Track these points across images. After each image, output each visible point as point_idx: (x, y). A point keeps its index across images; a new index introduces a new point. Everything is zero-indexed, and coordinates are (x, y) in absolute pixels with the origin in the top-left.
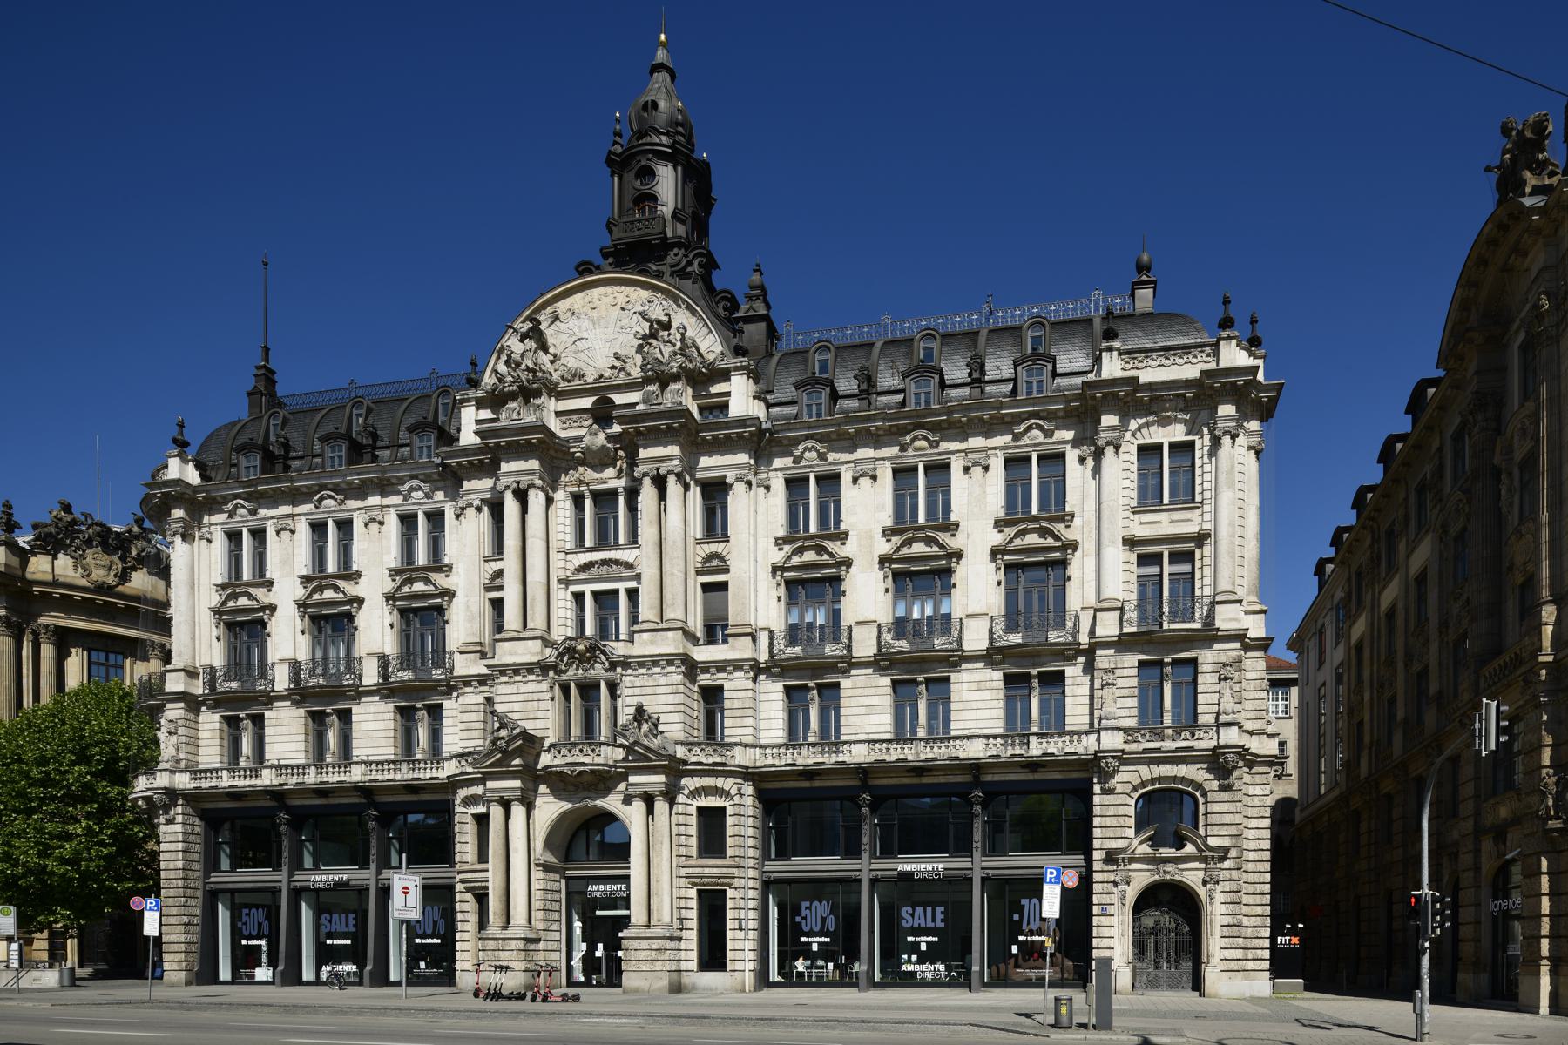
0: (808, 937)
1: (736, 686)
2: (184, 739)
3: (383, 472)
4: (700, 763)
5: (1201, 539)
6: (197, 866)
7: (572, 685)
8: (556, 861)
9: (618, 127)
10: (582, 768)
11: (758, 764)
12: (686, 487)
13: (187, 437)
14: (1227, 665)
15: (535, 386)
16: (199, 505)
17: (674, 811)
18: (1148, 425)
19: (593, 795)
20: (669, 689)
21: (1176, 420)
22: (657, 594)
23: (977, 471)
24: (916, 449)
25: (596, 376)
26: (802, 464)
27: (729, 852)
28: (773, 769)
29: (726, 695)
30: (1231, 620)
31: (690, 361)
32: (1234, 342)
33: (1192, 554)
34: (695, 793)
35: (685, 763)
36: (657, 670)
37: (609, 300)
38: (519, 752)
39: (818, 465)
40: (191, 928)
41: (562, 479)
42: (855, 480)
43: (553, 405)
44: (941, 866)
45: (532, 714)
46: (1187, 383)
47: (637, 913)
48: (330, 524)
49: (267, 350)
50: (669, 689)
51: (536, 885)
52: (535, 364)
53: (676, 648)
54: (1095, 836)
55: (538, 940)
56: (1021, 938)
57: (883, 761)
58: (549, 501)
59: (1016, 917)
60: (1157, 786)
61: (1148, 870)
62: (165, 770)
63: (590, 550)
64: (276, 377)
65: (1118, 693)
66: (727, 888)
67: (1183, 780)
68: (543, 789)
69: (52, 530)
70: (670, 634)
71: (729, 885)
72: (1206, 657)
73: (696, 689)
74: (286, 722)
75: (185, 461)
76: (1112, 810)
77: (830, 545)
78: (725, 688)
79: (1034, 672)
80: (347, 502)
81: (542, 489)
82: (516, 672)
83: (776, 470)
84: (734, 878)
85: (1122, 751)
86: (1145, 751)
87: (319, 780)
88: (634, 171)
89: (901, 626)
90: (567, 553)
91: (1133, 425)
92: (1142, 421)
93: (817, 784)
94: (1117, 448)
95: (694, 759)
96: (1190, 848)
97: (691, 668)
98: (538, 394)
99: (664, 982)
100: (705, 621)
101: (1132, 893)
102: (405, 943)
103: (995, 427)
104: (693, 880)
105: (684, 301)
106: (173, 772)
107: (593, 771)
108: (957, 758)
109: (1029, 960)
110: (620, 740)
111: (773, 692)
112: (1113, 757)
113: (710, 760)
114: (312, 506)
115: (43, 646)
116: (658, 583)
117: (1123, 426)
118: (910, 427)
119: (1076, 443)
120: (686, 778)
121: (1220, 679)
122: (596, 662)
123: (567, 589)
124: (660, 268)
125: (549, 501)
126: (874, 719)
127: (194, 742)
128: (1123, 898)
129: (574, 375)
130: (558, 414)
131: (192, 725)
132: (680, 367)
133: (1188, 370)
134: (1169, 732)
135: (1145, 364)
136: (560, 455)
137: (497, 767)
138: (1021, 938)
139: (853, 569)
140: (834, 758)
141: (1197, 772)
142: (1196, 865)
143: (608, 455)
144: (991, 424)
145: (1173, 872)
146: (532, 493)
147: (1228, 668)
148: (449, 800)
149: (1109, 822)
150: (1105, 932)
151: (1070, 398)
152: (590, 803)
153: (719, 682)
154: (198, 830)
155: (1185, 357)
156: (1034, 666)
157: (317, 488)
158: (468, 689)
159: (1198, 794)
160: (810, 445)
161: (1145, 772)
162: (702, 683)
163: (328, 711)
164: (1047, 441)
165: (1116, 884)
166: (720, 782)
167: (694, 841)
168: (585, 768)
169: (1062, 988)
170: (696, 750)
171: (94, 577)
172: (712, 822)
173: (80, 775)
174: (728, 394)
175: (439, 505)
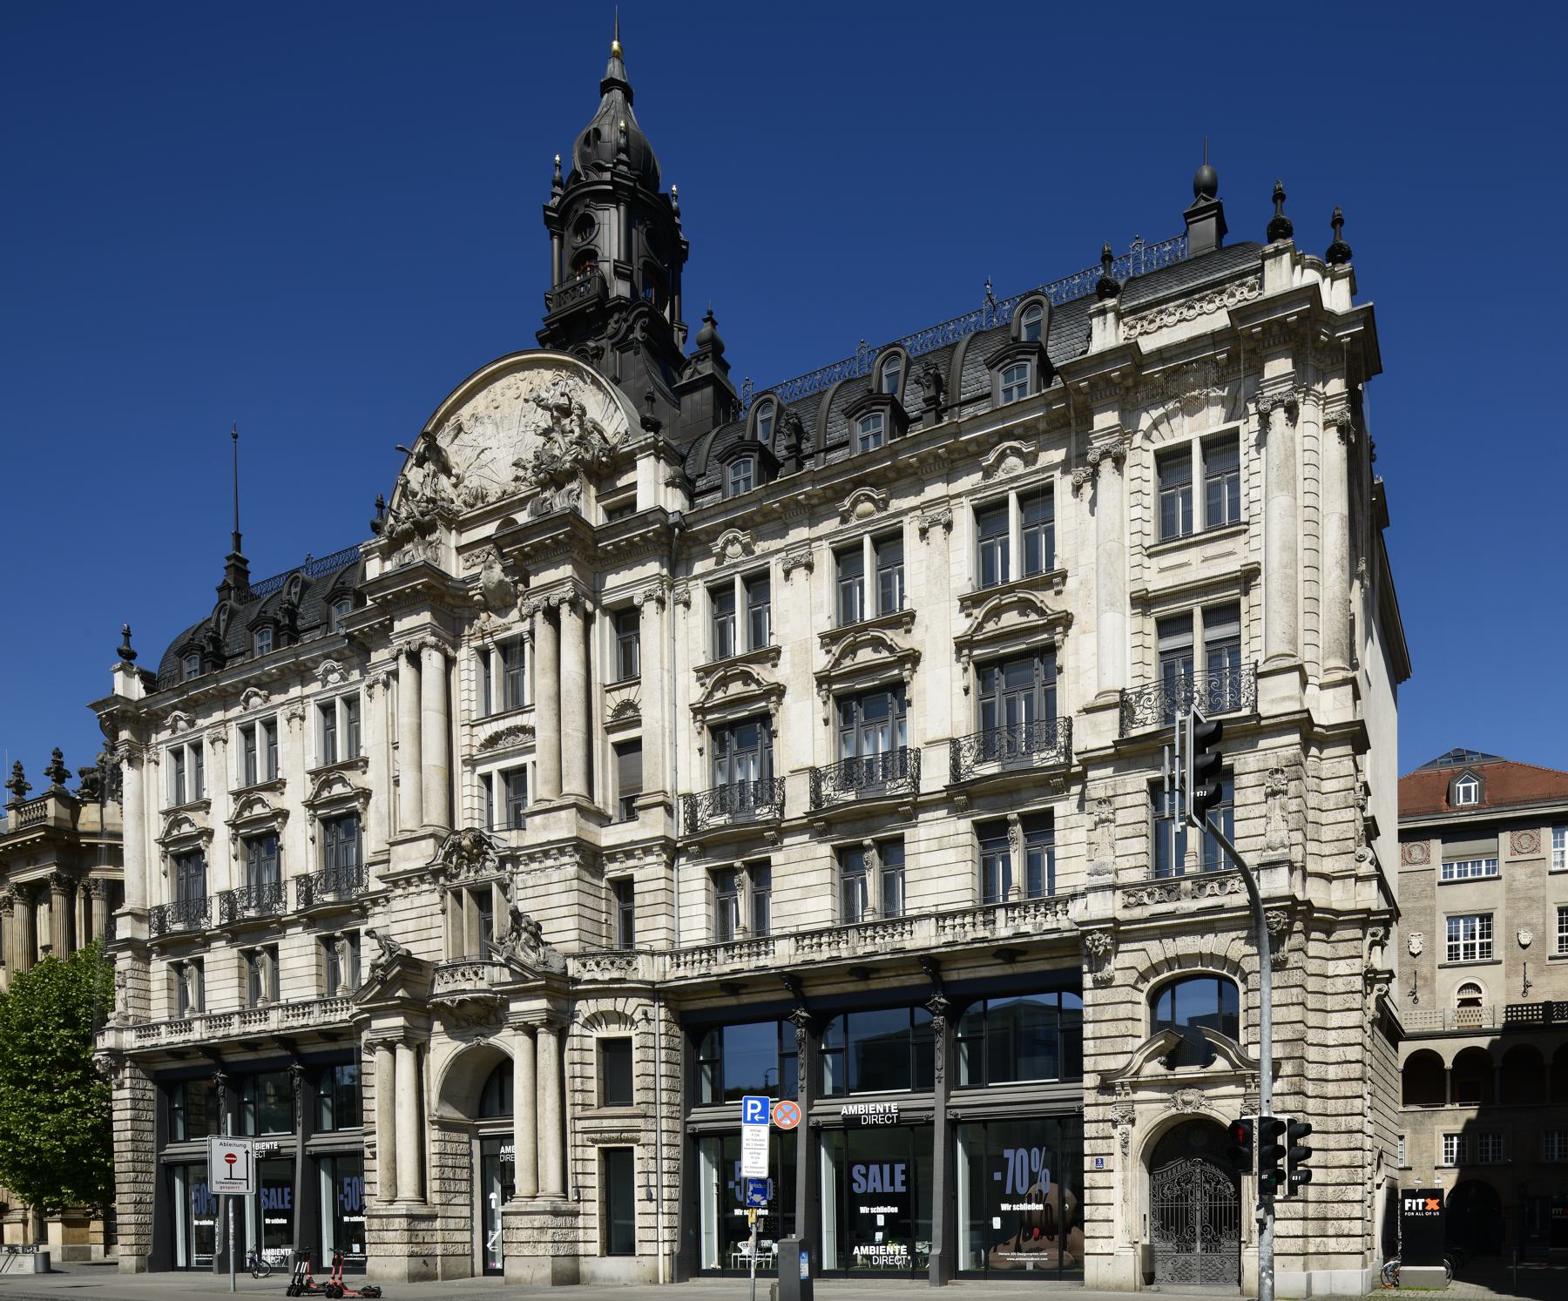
0: (1011, 1203)
1: (648, 873)
2: (131, 993)
3: (297, 656)
5: (1247, 578)
6: (151, 1137)
7: (465, 891)
8: (462, 1117)
9: (557, 174)
10: (461, 997)
12: (588, 620)
13: (134, 647)
14: (1277, 771)
15: (427, 518)
16: (144, 721)
17: (568, 1046)
18: (1168, 417)
19: (486, 1031)
20: (561, 887)
21: (1209, 402)
22: (554, 764)
23: (937, 532)
24: (860, 517)
25: (500, 494)
26: (725, 564)
27: (637, 1097)
28: (683, 982)
29: (637, 888)
30: (1284, 699)
31: (587, 450)
32: (1286, 257)
33: (1235, 605)
34: (593, 1021)
35: (577, 981)
36: (550, 862)
37: (513, 393)
38: (400, 981)
39: (743, 562)
40: (143, 1207)
41: (466, 633)
42: (787, 573)
43: (453, 539)
44: (894, 1106)
45: (423, 934)
46: (1214, 338)
48: (258, 725)
49: (238, 536)
50: (561, 887)
51: (432, 1148)
52: (436, 492)
53: (569, 832)
54: (1085, 1052)
55: (433, 1217)
56: (1005, 1207)
57: (812, 962)
58: (449, 663)
59: (998, 1176)
60: (1177, 971)
61: (1162, 1101)
62: (112, 1028)
63: (497, 717)
64: (249, 567)
65: (1120, 832)
66: (635, 1145)
67: (1212, 958)
68: (437, 1026)
69: (98, 775)
70: (563, 814)
71: (636, 1141)
72: (1246, 763)
73: (603, 884)
74: (222, 965)
75: (129, 674)
76: (1108, 1013)
77: (755, 670)
78: (636, 880)
79: (1012, 816)
80: (272, 698)
81: (436, 647)
82: (408, 882)
83: (696, 578)
84: (640, 1131)
85: (1114, 920)
87: (242, 1030)
88: (571, 229)
89: (850, 772)
90: (472, 726)
91: (1145, 421)
92: (1155, 413)
93: (745, 999)
94: (1119, 461)
95: (587, 976)
96: (1220, 1064)
97: (591, 858)
98: (432, 528)
99: (546, 1271)
100: (621, 793)
101: (1138, 1136)
102: (231, 1223)
103: (960, 463)
104: (593, 1136)
105: (588, 373)
106: (119, 1030)
107: (474, 1000)
108: (902, 950)
109: (1029, 1238)
110: (496, 958)
111: (694, 877)
112: (1101, 930)
113: (607, 976)
114: (241, 708)
115: (95, 903)
116: (555, 749)
117: (1126, 428)
118: (848, 486)
119: (1066, 467)
120: (580, 1002)
121: (1267, 795)
122: (485, 860)
123: (473, 771)
124: (599, 344)
125: (449, 663)
126: (811, 904)
127: (144, 995)
128: (1125, 1144)
129: (476, 498)
130: (460, 550)
131: (142, 975)
132: (575, 460)
133: (1212, 318)
134: (1187, 885)
135: (1158, 323)
136: (458, 602)
137: (380, 1001)
138: (1005, 1207)
139: (787, 699)
140: (755, 962)
141: (1230, 945)
142: (1231, 1089)
143: (508, 593)
144: (953, 461)
145: (1196, 1102)
146: (425, 654)
147: (1279, 776)
148: (351, 1050)
149: (1105, 1029)
150: (1101, 1196)
151: (1050, 398)
152: (483, 1042)
153: (629, 872)
154: (150, 1095)
155: (1217, 300)
156: (1012, 807)
157: (241, 685)
158: (378, 909)
159: (1236, 979)
160: (731, 536)
161: (1157, 950)
162: (611, 875)
163: (258, 949)
164: (1028, 470)
165: (1115, 1124)
166: (620, 1005)
167: (593, 1085)
168: (465, 997)
169: (1060, 1279)
170: (591, 963)
172: (615, 1054)
173: (61, 1039)
174: (633, 486)
175: (354, 687)
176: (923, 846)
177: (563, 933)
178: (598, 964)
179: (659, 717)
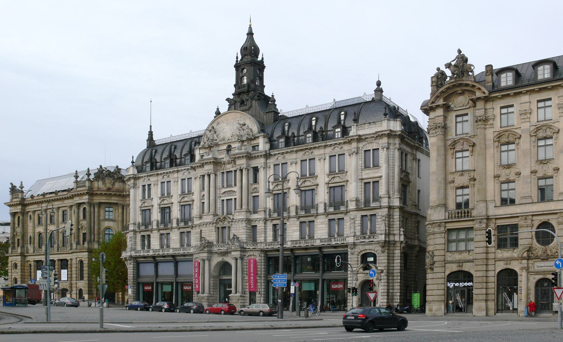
1: (260, 226)
4: (249, 249)
11: (265, 248)
29: (258, 228)
35: (246, 249)
38: (207, 246)
47: (233, 289)
49: (151, 126)
52: (213, 138)
63: (226, 188)
64: (153, 133)
86: (361, 242)
95: (248, 248)
97: (249, 221)
113: (252, 248)
132: (247, 138)
171: (107, 186)
174: (259, 143)
176: (318, 223)
177: (243, 237)
178: (250, 245)
179: (274, 217)
